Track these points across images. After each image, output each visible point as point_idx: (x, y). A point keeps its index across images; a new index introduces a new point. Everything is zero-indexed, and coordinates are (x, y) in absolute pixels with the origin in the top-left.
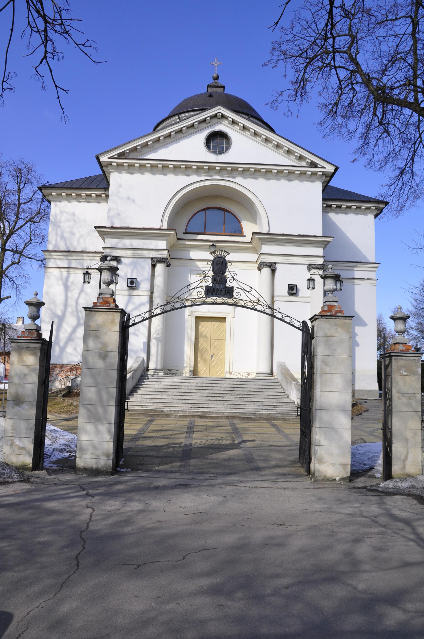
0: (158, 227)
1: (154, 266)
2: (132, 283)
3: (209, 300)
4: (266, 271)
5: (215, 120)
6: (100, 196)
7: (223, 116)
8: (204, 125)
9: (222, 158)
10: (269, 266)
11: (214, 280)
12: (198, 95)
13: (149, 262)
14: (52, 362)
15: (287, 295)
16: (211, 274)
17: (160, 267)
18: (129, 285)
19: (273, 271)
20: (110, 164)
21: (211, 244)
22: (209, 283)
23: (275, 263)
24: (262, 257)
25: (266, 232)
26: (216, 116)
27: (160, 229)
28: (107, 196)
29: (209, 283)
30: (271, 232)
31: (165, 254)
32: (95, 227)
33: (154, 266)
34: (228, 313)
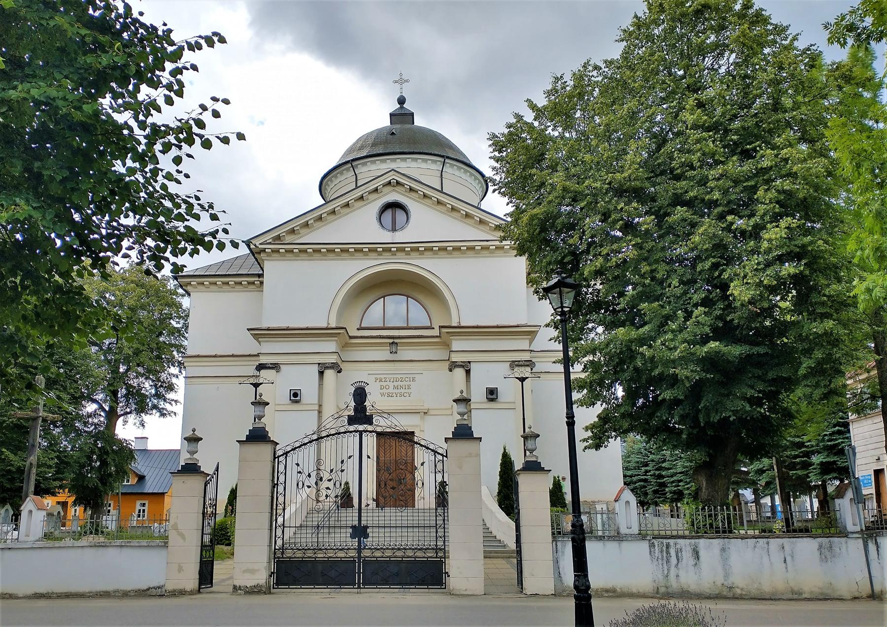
0: (325, 325)
1: (321, 373)
2: (295, 395)
3: (352, 428)
4: (460, 373)
5: (389, 188)
6: (253, 283)
7: (398, 183)
8: (375, 196)
9: (400, 237)
10: (462, 366)
11: (356, 409)
12: (380, 131)
13: (316, 369)
14: (581, 499)
15: (486, 400)
16: (353, 404)
17: (329, 374)
18: (292, 398)
19: (468, 372)
20: (264, 250)
21: (391, 341)
22: (352, 413)
23: (469, 362)
24: (453, 355)
25: (456, 325)
26: (389, 183)
27: (327, 329)
28: (262, 283)
29: (352, 413)
30: (463, 324)
31: (332, 359)
32: (248, 330)
33: (321, 373)
34: (417, 426)
